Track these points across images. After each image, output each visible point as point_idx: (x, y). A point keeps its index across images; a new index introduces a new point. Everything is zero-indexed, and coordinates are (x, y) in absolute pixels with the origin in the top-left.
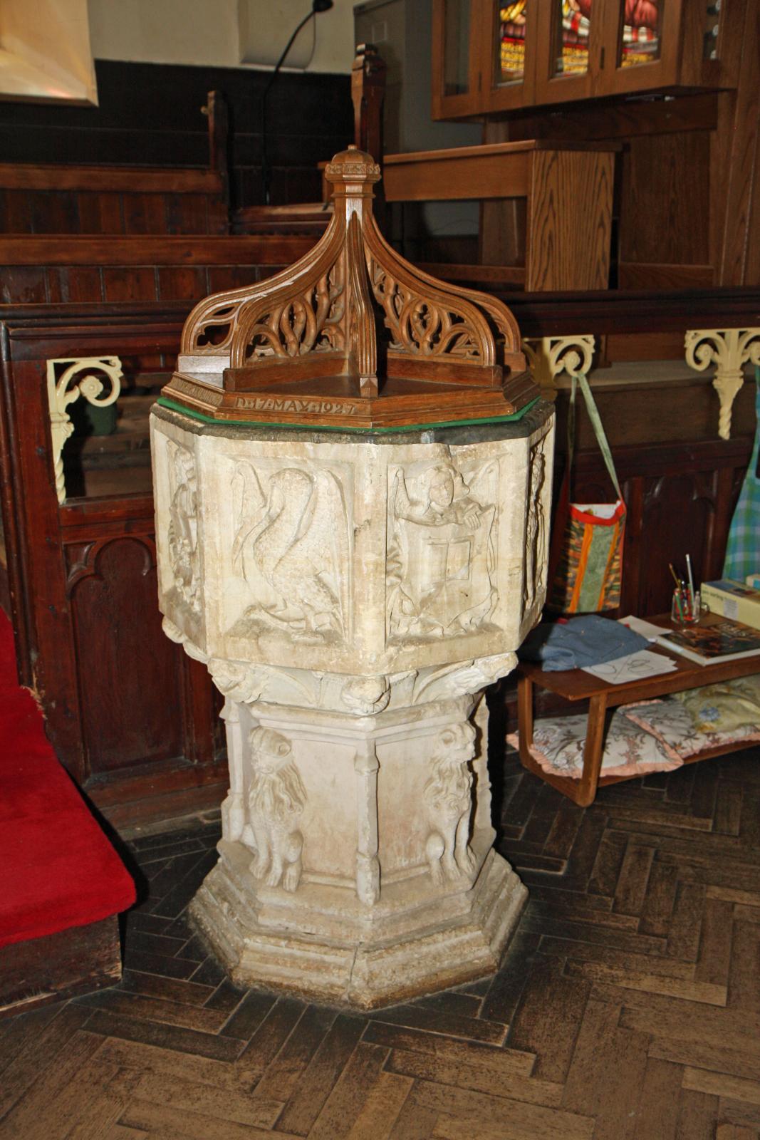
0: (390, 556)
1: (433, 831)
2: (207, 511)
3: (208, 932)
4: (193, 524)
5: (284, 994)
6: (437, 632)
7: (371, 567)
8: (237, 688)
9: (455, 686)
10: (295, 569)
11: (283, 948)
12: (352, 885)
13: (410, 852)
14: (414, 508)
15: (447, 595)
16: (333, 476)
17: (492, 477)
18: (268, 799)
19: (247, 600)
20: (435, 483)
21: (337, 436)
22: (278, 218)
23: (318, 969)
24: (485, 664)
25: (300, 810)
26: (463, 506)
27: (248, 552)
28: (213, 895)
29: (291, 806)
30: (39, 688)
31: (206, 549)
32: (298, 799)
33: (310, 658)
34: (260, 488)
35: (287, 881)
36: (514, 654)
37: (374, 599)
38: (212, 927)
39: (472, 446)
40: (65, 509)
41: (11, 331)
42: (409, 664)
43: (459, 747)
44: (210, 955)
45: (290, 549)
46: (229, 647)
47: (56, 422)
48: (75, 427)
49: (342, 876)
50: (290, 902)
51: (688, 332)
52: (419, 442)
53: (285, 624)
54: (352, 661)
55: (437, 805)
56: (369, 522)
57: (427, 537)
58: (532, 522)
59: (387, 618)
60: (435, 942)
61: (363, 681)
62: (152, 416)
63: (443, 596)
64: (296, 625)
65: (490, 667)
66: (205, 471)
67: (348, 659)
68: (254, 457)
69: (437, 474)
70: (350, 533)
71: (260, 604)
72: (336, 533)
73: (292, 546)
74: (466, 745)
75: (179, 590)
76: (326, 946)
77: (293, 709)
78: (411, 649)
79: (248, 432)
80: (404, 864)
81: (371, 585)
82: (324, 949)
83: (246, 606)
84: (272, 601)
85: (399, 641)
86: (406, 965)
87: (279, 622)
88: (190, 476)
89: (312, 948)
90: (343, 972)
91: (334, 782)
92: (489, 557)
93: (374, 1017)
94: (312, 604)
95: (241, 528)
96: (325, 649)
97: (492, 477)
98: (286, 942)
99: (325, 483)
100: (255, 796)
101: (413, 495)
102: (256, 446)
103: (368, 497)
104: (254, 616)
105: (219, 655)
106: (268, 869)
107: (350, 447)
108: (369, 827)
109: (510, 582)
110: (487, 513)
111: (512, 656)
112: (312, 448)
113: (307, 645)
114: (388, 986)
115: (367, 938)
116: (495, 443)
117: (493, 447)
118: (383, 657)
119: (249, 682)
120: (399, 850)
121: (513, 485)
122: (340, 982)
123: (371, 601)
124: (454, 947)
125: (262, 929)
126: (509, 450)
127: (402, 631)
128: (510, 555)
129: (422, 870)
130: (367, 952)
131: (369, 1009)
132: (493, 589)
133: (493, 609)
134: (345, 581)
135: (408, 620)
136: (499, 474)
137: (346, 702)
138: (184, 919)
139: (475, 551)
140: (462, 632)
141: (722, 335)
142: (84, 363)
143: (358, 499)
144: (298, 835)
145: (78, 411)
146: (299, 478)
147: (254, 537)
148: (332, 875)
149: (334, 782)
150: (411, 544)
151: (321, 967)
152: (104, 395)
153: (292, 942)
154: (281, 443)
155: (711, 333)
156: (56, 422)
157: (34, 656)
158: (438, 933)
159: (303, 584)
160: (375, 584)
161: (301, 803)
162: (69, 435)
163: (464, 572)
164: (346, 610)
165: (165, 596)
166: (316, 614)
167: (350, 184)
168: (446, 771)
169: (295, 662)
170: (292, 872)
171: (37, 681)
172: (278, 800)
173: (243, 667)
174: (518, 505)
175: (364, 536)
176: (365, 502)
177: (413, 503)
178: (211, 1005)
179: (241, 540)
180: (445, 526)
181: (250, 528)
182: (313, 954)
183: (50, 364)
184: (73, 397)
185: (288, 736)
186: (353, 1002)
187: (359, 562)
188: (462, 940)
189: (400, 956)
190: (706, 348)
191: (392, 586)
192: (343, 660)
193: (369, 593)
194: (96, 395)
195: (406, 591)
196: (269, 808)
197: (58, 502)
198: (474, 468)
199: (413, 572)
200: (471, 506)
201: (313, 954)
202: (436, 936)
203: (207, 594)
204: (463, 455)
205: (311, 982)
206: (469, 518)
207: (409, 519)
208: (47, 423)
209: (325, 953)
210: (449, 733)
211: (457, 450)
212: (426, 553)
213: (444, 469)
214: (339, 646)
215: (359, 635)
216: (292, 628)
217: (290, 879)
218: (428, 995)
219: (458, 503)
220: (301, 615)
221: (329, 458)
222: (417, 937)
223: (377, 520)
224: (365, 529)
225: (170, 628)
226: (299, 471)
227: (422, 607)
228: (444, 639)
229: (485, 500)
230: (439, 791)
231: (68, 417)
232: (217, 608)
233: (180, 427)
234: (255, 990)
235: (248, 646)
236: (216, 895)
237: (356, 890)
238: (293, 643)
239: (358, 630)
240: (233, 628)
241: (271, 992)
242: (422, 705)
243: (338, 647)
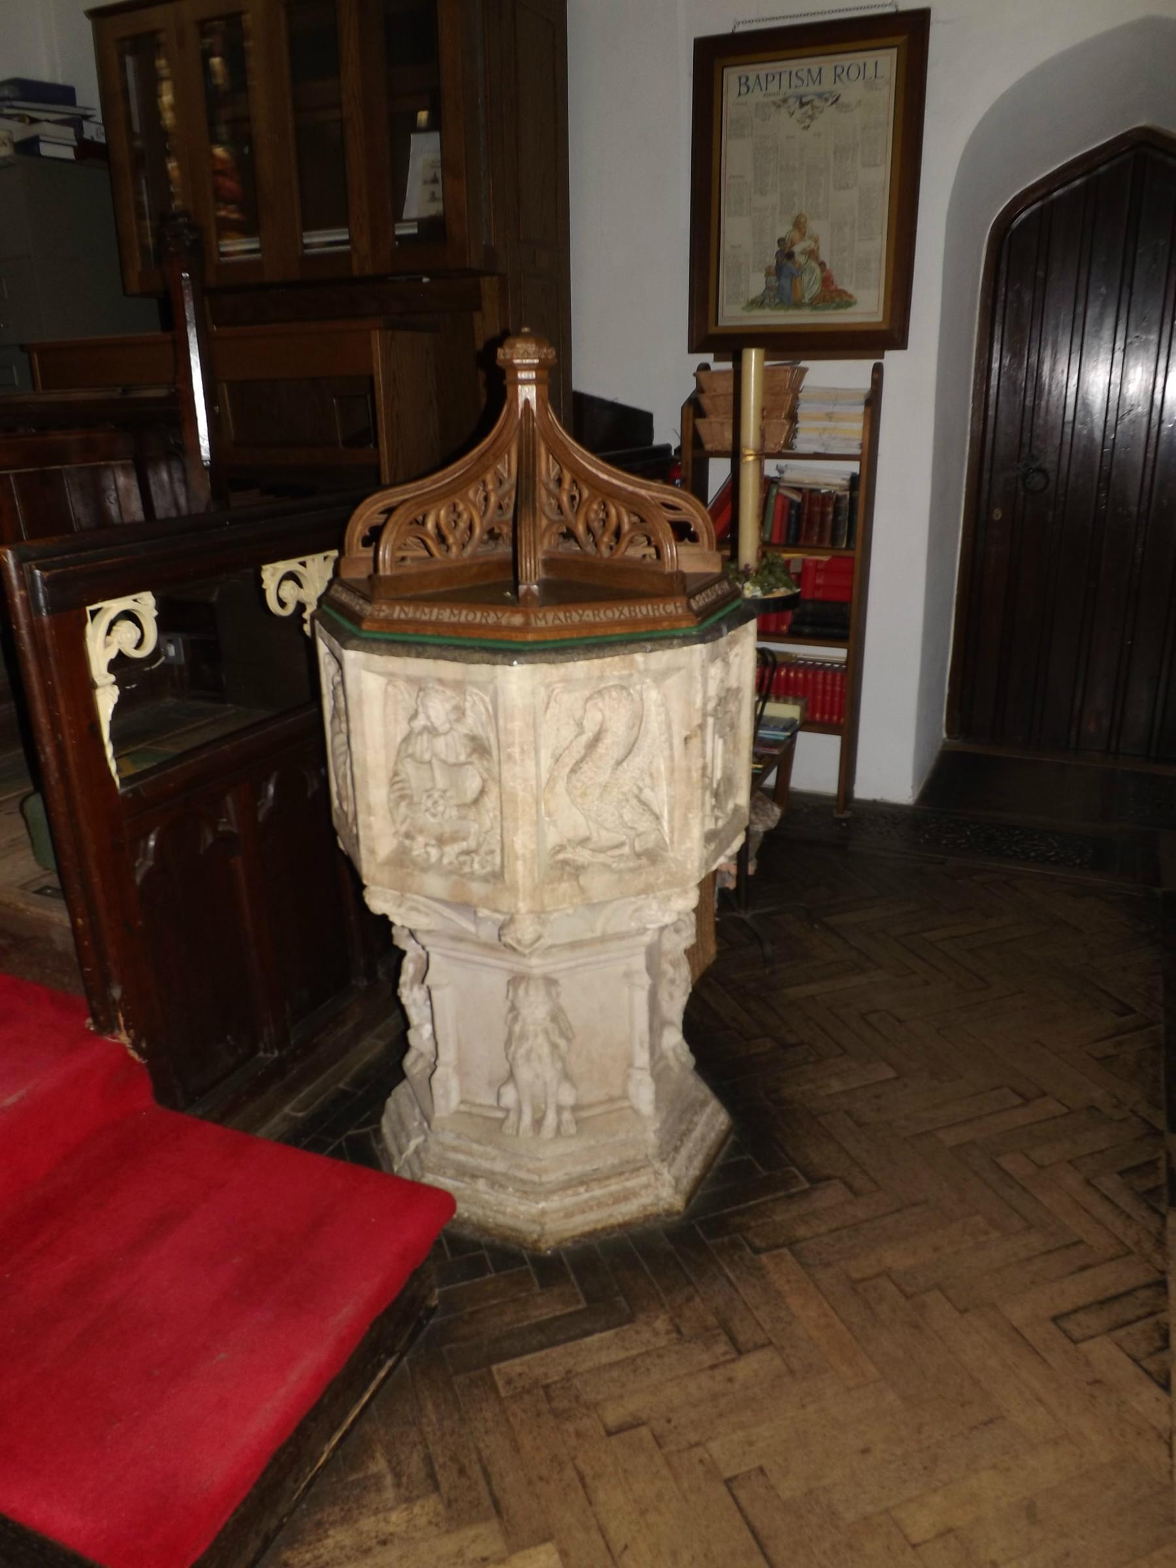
11: (584, 1195)
12: (626, 1104)
18: (546, 1050)
21: (667, 642)
38: (468, 1211)
40: (125, 795)
50: (574, 1146)
58: (342, 705)
64: (617, 852)
71: (569, 841)
82: (623, 1177)
84: (583, 832)
96: (652, 869)
102: (580, 668)
104: (561, 856)
145: (119, 665)
151: (624, 1197)
162: (116, 700)
167: (523, 370)
182: (614, 1186)
185: (555, 976)
186: (669, 1213)
189: (684, 1152)
201: (614, 1186)
208: (91, 686)
209: (627, 1180)
216: (612, 857)
222: (683, 1127)
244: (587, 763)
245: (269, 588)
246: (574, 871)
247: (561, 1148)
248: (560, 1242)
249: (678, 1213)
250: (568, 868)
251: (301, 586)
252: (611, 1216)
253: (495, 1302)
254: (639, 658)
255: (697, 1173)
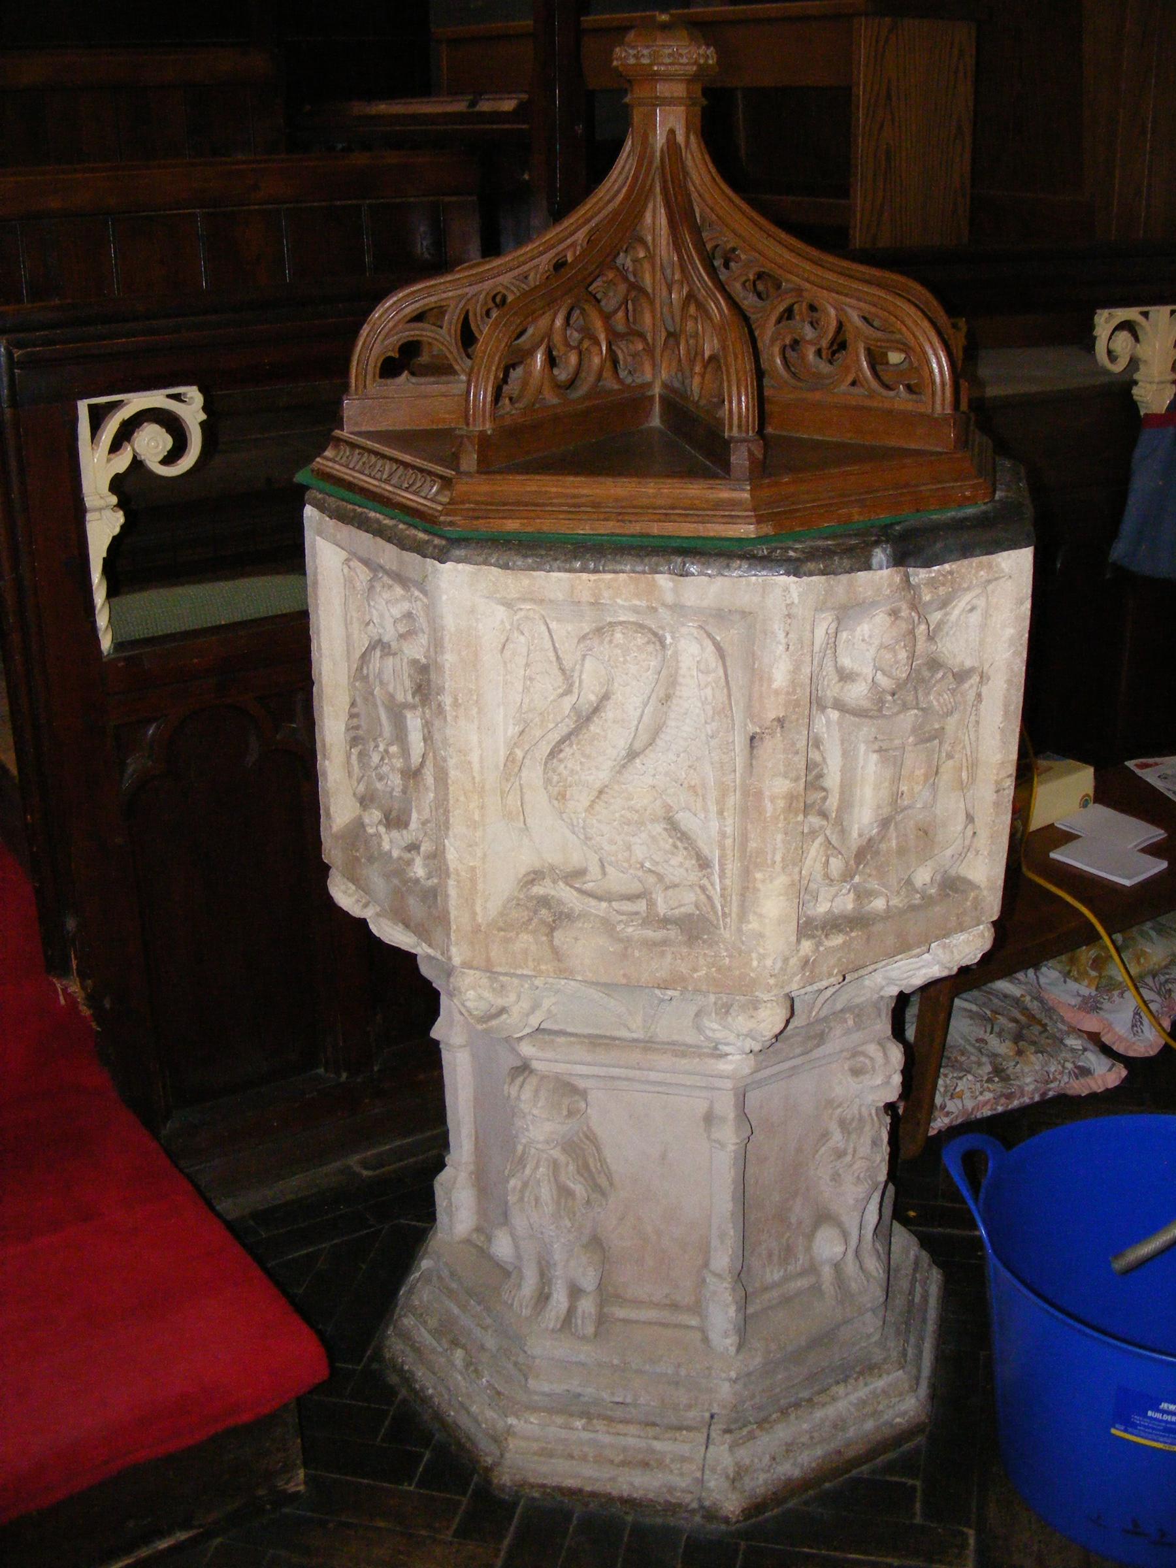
0: (813, 778)
1: (824, 1217)
2: (456, 704)
3: (431, 1397)
4: (414, 722)
5: (586, 1505)
6: (879, 904)
7: (781, 803)
8: (505, 1016)
9: (884, 983)
10: (630, 809)
12: (694, 1322)
13: (788, 1252)
14: (849, 686)
15: (897, 837)
16: (709, 636)
17: (975, 618)
18: (546, 1192)
19: (526, 860)
20: (887, 640)
22: (380, 117)
23: (646, 1465)
24: (944, 947)
25: (600, 1205)
26: (926, 674)
27: (533, 774)
28: (430, 1332)
29: (588, 1202)
30: (82, 976)
31: (453, 773)
32: (597, 1188)
33: (660, 967)
34: (558, 658)
35: (579, 1322)
36: (990, 926)
37: (783, 859)
38: (435, 1388)
39: (947, 566)
41: (17, 353)
42: (834, 966)
43: (879, 1082)
44: (437, 1436)
45: (619, 772)
46: (495, 952)
47: (95, 510)
48: (126, 515)
49: (675, 1307)
50: (586, 1353)
51: (1098, 311)
52: (869, 567)
53: (604, 905)
54: (737, 973)
55: (836, 1177)
56: (781, 721)
57: (871, 738)
59: (801, 892)
60: (834, 1399)
61: (755, 1005)
62: (309, 511)
63: (889, 840)
64: (627, 906)
65: (952, 952)
66: (453, 629)
67: (729, 969)
68: (551, 601)
69: (893, 623)
70: (739, 741)
71: (552, 868)
72: (713, 743)
73: (624, 766)
74: (890, 1077)
75: (371, 830)
76: (654, 1424)
77: (596, 1042)
78: (837, 940)
79: (542, 556)
80: (777, 1276)
81: (779, 837)
82: (651, 1431)
83: (523, 871)
84: (576, 859)
85: (816, 928)
86: (792, 1444)
87: (593, 902)
88: (402, 630)
89: (632, 1429)
90: (687, 1467)
91: (663, 1157)
92: (965, 764)
93: (747, 1535)
94: (659, 869)
95: (522, 733)
96: (685, 950)
97: (975, 618)
98: (584, 1421)
99: (694, 648)
100: (519, 1184)
101: (846, 662)
103: (780, 676)
104: (538, 890)
105: (475, 963)
106: (543, 1297)
107: (748, 584)
108: (732, 1233)
109: (997, 804)
110: (966, 686)
111: (989, 930)
112: (671, 584)
113: (650, 945)
114: (766, 1482)
115: (724, 1407)
116: (985, 558)
117: (980, 567)
118: (793, 961)
119: (525, 1005)
120: (770, 1255)
121: (1010, 632)
122: (682, 1483)
123: (778, 866)
124: (863, 1403)
125: (536, 1398)
126: (1007, 570)
127: (822, 908)
128: (998, 757)
129: (802, 1283)
130: (728, 1431)
131: (737, 1522)
132: (970, 818)
133: (961, 856)
134: (729, 830)
135: (833, 890)
136: (987, 615)
137: (709, 1033)
138: (375, 1366)
139: (944, 754)
140: (917, 899)
141: (1145, 315)
142: (137, 402)
143: (761, 679)
144: (596, 1244)
146: (640, 640)
147: (545, 749)
148: (657, 1305)
149: (663, 1157)
150: (845, 754)
152: (171, 458)
153: (595, 1421)
154: (609, 576)
155: (1131, 313)
156: (95, 510)
157: (71, 924)
158: (838, 1383)
159: (644, 836)
160: (786, 834)
161: (603, 1194)
163: (926, 794)
164: (728, 882)
165: (337, 837)
166: (667, 888)
168: (853, 1120)
169: (624, 975)
170: (587, 1305)
171: (77, 965)
172: (564, 1192)
173: (516, 981)
174: (1016, 669)
175: (773, 751)
176: (775, 686)
177: (845, 676)
178: (463, 1533)
179: (519, 753)
180: (902, 716)
181: (538, 733)
183: (83, 407)
184: (122, 462)
185: (581, 1084)
186: (710, 1514)
187: (759, 794)
188: (876, 1389)
189: (782, 1433)
190: (1124, 336)
191: (813, 833)
192: (719, 970)
193: (774, 850)
194: (160, 457)
195: (834, 840)
196: (549, 1209)
197: (101, 652)
198: (944, 604)
199: (846, 804)
200: (940, 675)
201: (633, 1439)
202: (834, 1389)
203: (451, 855)
204: (932, 583)
205: (632, 1484)
206: (936, 700)
207: (839, 706)
208: (78, 511)
209: (656, 1438)
210: (862, 1059)
211: (920, 575)
212: (870, 766)
213: (904, 613)
214: (711, 944)
215: (753, 925)
217: (583, 1318)
218: (827, 1485)
219: (918, 671)
220: (636, 887)
221: (705, 604)
222: (805, 1394)
223: (794, 717)
224: (772, 735)
225: (345, 892)
226: (641, 627)
227: (858, 864)
228: (888, 915)
229: (958, 660)
230: (840, 1154)
231: (114, 500)
232: (473, 880)
233: (389, 540)
234: (533, 1499)
235: (533, 948)
236: (437, 1333)
237: (702, 1330)
238: (620, 940)
239: (751, 917)
240: (501, 914)
241: (562, 1502)
242: (825, 1019)
243: (711, 946)
244: (571, 745)
245: (1100, 336)
246: (561, 917)
247: (562, 1349)
248: (523, 1484)
249: (726, 1520)
250: (544, 911)
251: (1137, 339)
252: (613, 1479)
253: (382, 1524)
254: (664, 581)
255: (797, 1473)
